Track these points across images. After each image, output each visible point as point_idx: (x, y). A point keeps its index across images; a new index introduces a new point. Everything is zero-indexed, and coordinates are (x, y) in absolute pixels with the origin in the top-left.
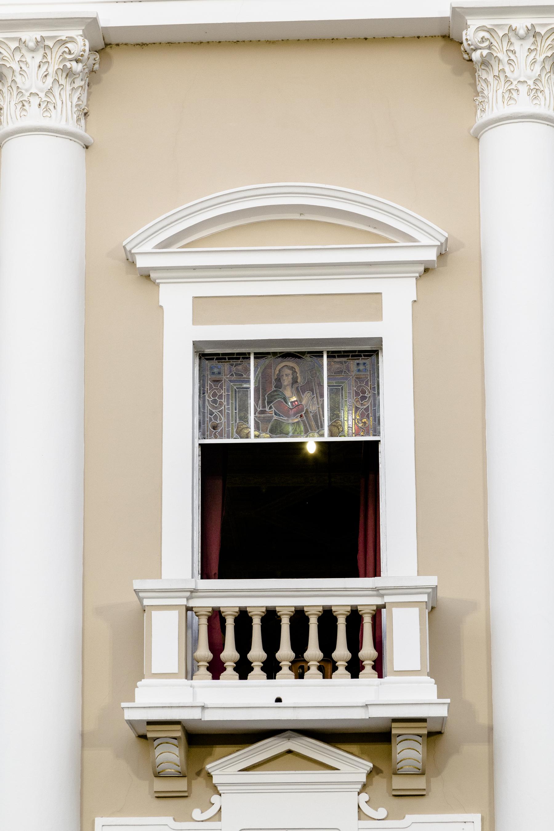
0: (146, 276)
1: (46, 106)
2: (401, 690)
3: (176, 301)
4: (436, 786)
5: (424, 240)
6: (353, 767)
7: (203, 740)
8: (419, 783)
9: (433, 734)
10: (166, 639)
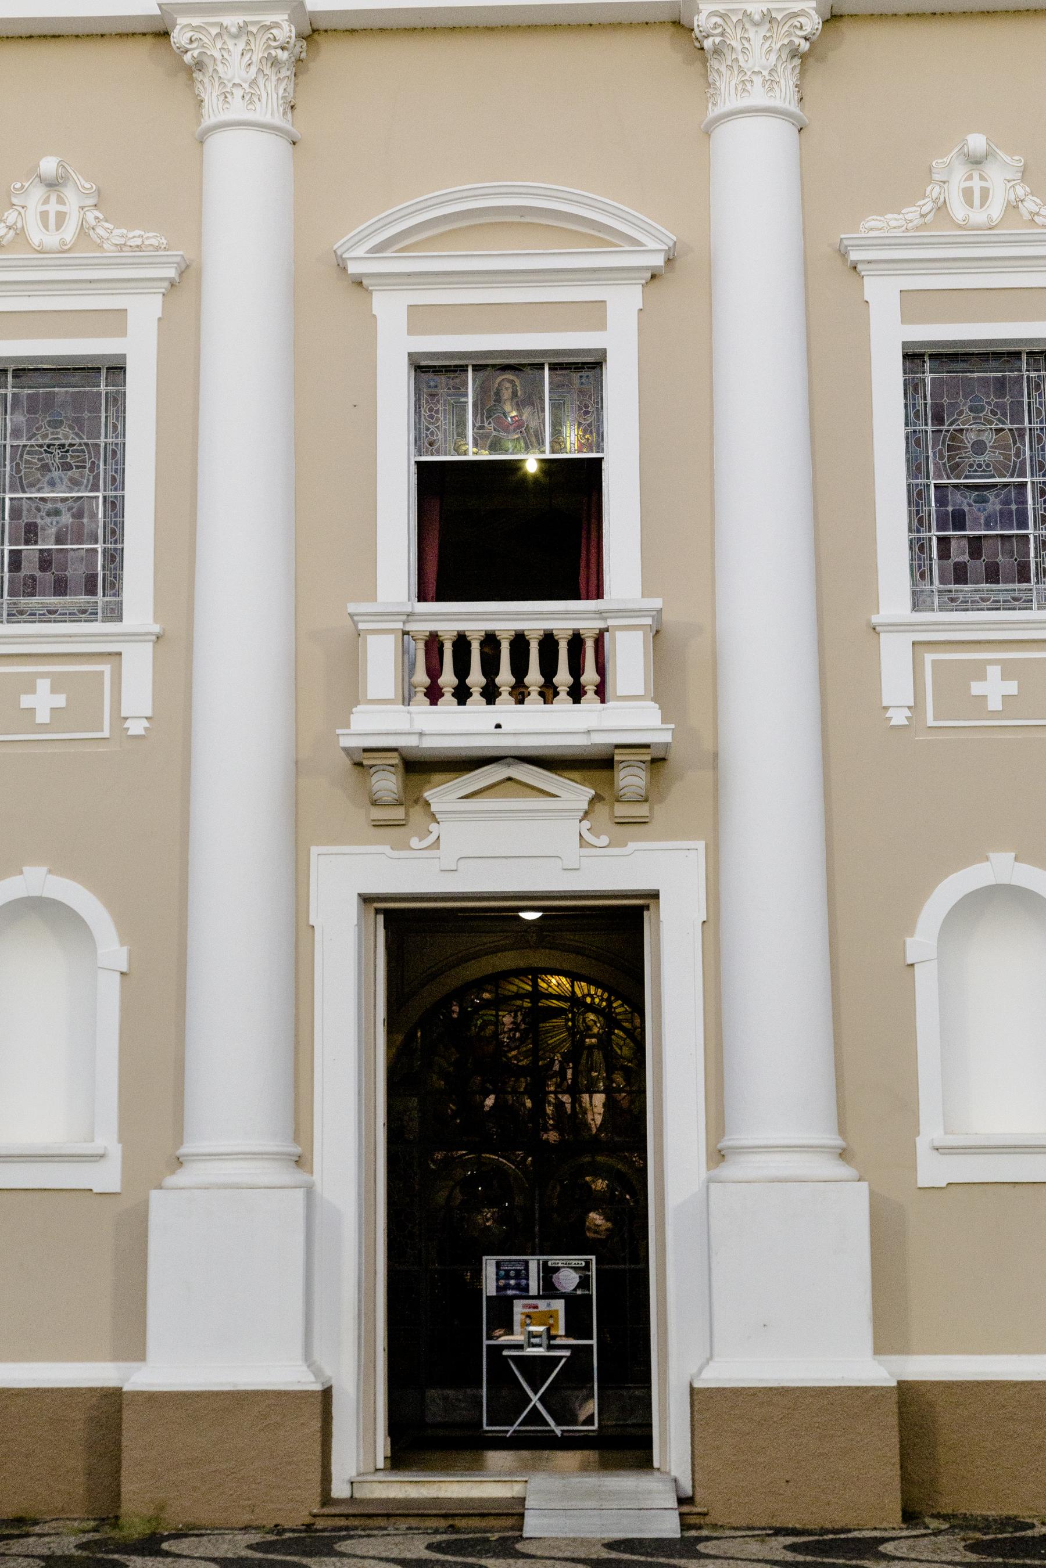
0: (358, 283)
1: (251, 98)
2: (623, 715)
3: (389, 309)
4: (660, 812)
6: (574, 793)
7: (420, 768)
8: (642, 810)
10: (382, 663)
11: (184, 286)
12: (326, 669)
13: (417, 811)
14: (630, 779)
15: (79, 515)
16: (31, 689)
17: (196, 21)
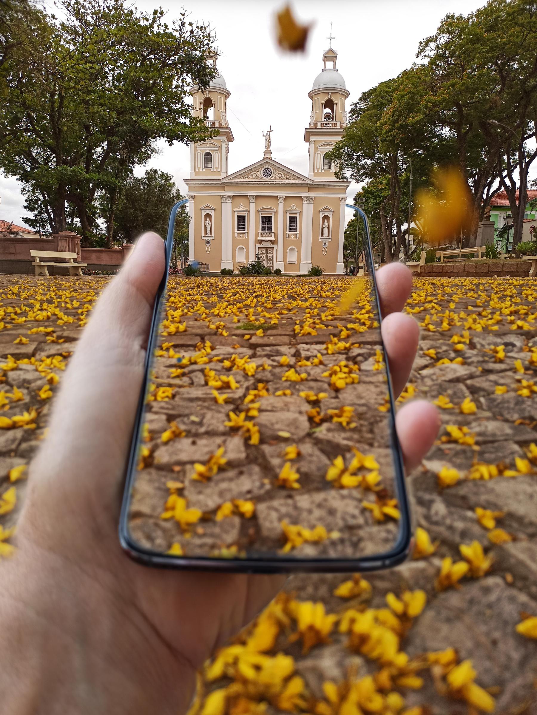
2: (273, 238)
7: (262, 241)
11: (249, 212)
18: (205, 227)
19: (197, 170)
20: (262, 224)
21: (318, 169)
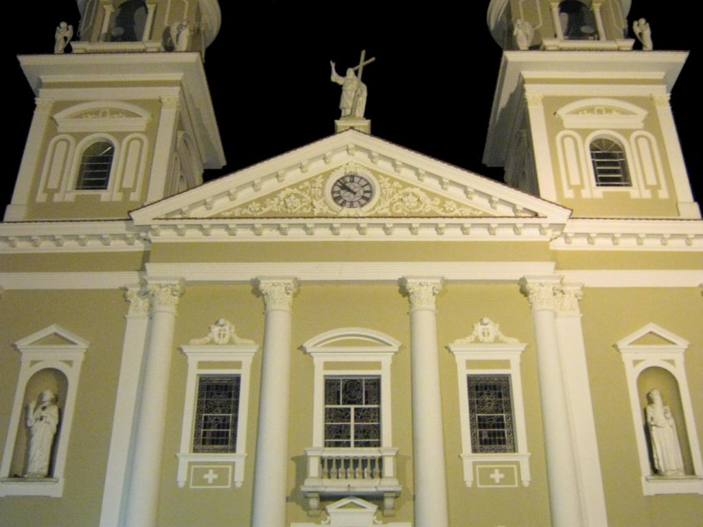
2: (388, 483)
5: (395, 345)
6: (371, 507)
7: (326, 498)
9: (397, 495)
10: (314, 467)
12: (300, 465)
13: (323, 512)
14: (388, 502)
15: (224, 421)
16: (207, 473)
17: (267, 282)
18: (26, 432)
19: (41, 197)
20: (329, 414)
21: (50, 193)
